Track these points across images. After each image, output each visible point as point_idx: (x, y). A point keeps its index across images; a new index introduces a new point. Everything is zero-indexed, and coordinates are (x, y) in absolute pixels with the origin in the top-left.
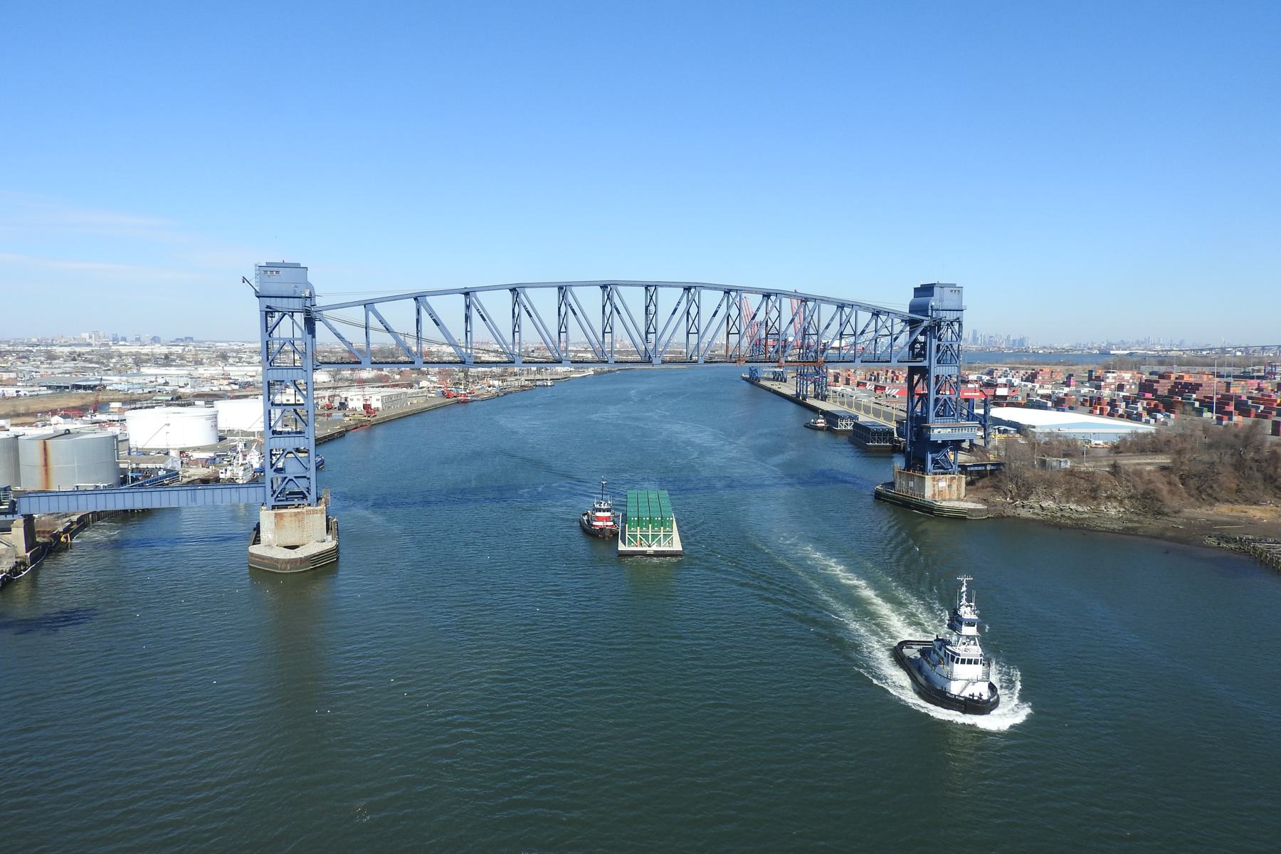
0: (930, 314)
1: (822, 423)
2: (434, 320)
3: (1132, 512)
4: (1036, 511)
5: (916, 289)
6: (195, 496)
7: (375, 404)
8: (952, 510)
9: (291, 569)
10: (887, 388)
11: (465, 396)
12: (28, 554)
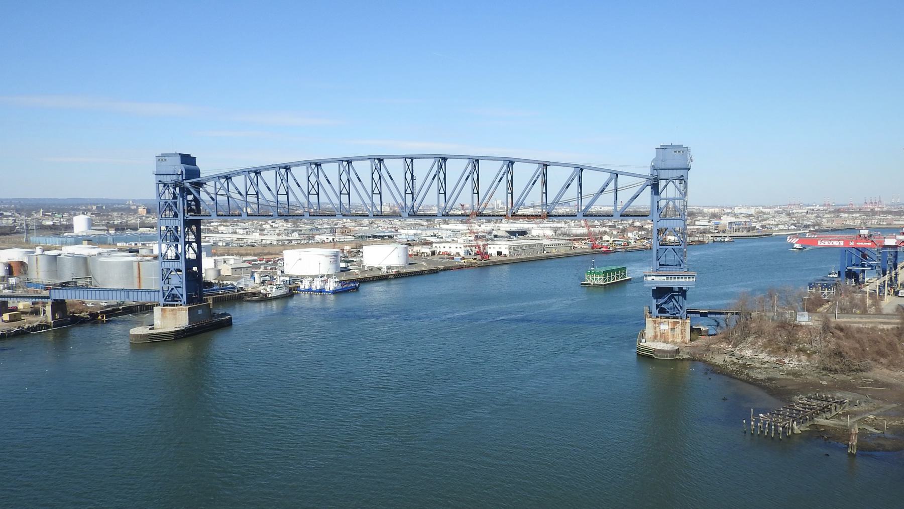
2: (567, 188)
6: (129, 293)
7: (505, 252)
11: (607, 248)
12: (53, 321)
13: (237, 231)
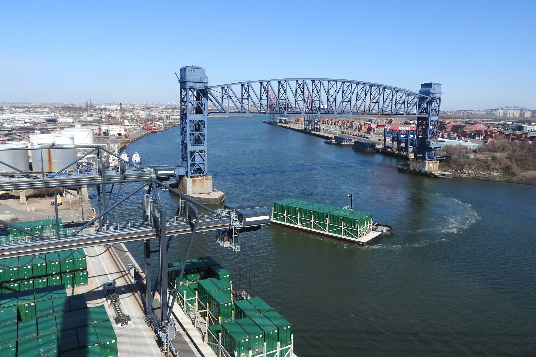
0: (430, 96)
1: (334, 141)
3: (502, 174)
4: (467, 175)
5: (422, 85)
8: (439, 175)
9: (214, 203)
10: (386, 126)
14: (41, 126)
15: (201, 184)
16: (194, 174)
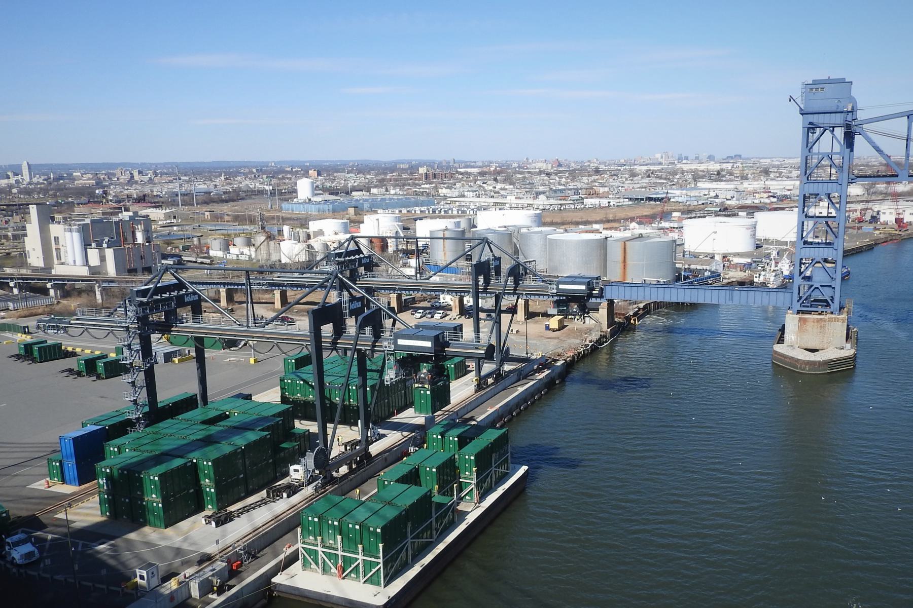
9: (809, 370)
12: (609, 330)
13: (466, 193)
14: (792, 202)
15: (819, 328)
16: (808, 307)
